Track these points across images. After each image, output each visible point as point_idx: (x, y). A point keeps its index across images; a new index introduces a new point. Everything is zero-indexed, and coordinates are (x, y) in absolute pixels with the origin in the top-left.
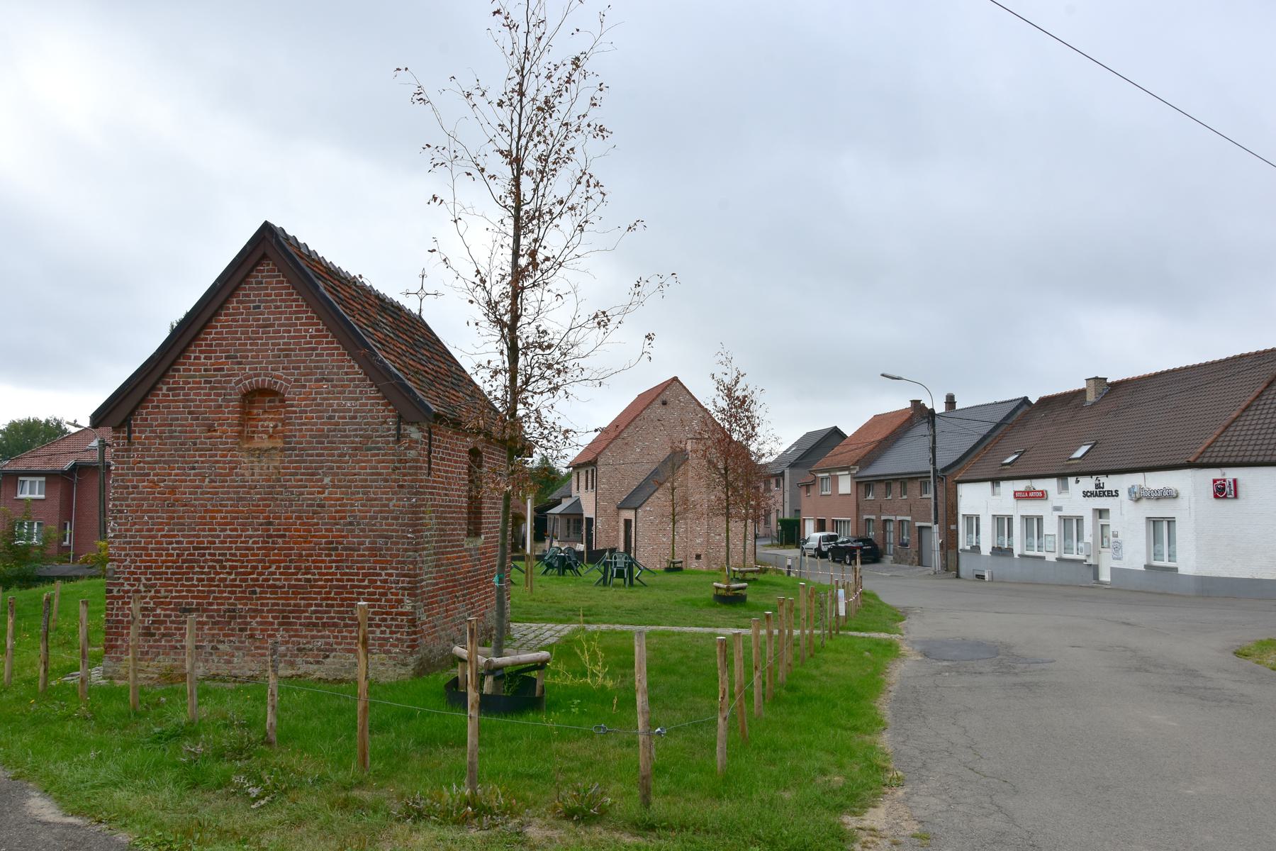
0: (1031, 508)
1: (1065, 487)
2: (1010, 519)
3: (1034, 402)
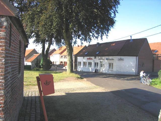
0: (90, 61)
1: (95, 58)
2: (86, 63)
3: (87, 46)
